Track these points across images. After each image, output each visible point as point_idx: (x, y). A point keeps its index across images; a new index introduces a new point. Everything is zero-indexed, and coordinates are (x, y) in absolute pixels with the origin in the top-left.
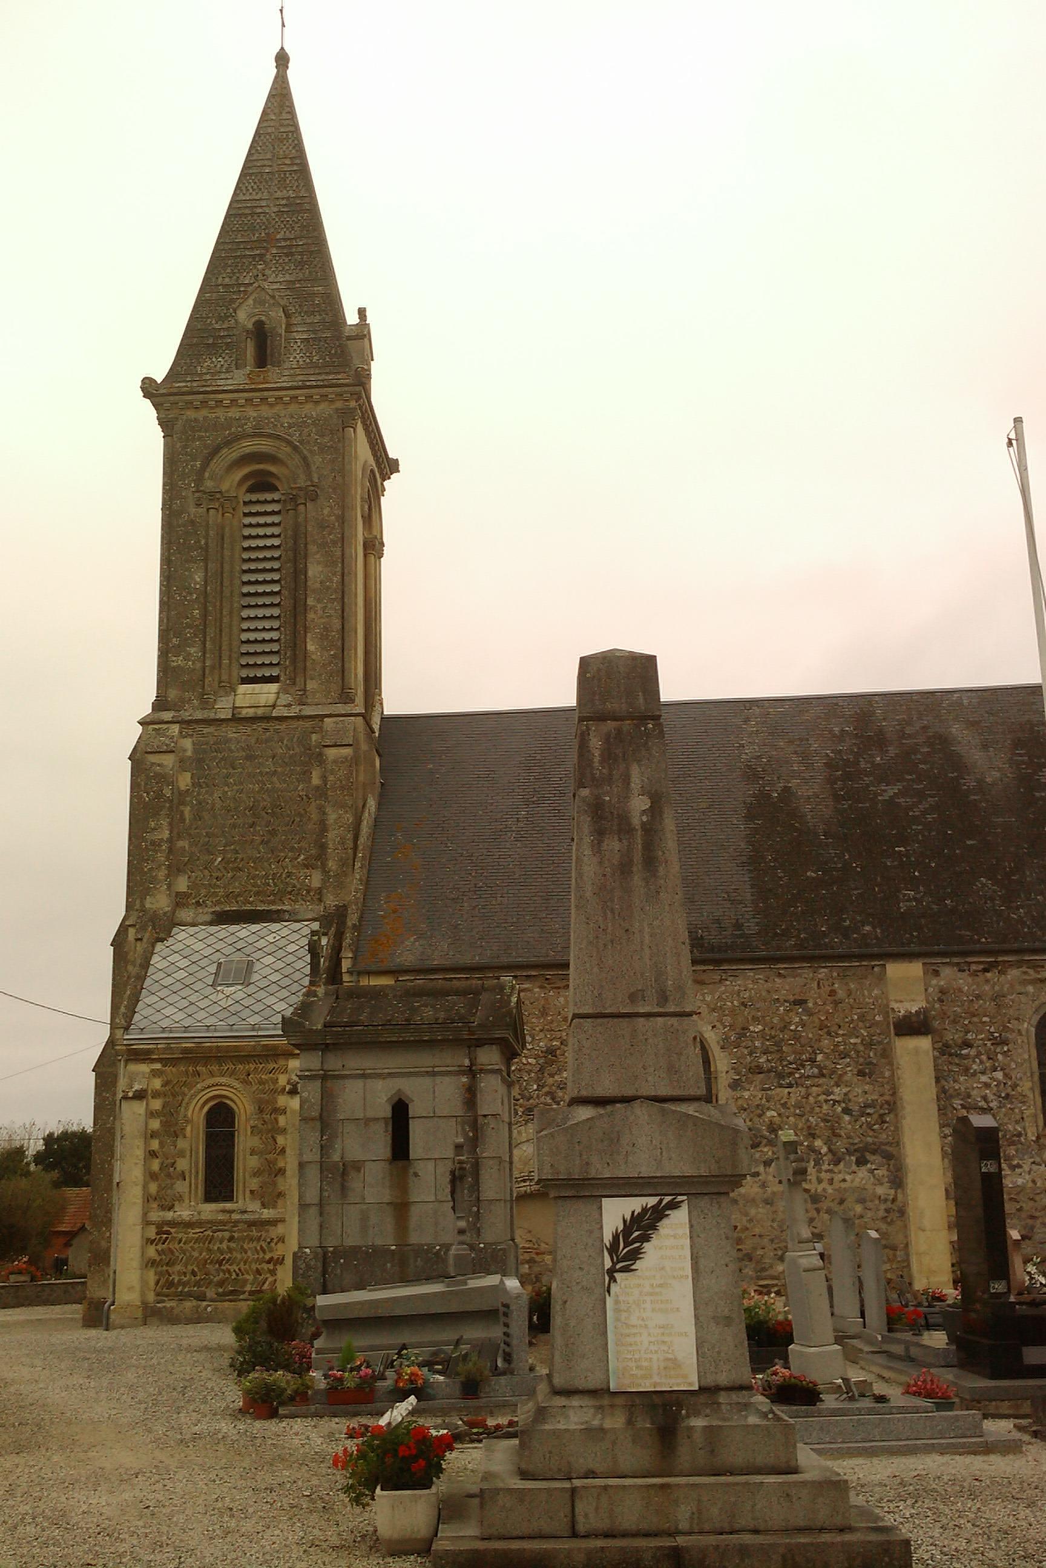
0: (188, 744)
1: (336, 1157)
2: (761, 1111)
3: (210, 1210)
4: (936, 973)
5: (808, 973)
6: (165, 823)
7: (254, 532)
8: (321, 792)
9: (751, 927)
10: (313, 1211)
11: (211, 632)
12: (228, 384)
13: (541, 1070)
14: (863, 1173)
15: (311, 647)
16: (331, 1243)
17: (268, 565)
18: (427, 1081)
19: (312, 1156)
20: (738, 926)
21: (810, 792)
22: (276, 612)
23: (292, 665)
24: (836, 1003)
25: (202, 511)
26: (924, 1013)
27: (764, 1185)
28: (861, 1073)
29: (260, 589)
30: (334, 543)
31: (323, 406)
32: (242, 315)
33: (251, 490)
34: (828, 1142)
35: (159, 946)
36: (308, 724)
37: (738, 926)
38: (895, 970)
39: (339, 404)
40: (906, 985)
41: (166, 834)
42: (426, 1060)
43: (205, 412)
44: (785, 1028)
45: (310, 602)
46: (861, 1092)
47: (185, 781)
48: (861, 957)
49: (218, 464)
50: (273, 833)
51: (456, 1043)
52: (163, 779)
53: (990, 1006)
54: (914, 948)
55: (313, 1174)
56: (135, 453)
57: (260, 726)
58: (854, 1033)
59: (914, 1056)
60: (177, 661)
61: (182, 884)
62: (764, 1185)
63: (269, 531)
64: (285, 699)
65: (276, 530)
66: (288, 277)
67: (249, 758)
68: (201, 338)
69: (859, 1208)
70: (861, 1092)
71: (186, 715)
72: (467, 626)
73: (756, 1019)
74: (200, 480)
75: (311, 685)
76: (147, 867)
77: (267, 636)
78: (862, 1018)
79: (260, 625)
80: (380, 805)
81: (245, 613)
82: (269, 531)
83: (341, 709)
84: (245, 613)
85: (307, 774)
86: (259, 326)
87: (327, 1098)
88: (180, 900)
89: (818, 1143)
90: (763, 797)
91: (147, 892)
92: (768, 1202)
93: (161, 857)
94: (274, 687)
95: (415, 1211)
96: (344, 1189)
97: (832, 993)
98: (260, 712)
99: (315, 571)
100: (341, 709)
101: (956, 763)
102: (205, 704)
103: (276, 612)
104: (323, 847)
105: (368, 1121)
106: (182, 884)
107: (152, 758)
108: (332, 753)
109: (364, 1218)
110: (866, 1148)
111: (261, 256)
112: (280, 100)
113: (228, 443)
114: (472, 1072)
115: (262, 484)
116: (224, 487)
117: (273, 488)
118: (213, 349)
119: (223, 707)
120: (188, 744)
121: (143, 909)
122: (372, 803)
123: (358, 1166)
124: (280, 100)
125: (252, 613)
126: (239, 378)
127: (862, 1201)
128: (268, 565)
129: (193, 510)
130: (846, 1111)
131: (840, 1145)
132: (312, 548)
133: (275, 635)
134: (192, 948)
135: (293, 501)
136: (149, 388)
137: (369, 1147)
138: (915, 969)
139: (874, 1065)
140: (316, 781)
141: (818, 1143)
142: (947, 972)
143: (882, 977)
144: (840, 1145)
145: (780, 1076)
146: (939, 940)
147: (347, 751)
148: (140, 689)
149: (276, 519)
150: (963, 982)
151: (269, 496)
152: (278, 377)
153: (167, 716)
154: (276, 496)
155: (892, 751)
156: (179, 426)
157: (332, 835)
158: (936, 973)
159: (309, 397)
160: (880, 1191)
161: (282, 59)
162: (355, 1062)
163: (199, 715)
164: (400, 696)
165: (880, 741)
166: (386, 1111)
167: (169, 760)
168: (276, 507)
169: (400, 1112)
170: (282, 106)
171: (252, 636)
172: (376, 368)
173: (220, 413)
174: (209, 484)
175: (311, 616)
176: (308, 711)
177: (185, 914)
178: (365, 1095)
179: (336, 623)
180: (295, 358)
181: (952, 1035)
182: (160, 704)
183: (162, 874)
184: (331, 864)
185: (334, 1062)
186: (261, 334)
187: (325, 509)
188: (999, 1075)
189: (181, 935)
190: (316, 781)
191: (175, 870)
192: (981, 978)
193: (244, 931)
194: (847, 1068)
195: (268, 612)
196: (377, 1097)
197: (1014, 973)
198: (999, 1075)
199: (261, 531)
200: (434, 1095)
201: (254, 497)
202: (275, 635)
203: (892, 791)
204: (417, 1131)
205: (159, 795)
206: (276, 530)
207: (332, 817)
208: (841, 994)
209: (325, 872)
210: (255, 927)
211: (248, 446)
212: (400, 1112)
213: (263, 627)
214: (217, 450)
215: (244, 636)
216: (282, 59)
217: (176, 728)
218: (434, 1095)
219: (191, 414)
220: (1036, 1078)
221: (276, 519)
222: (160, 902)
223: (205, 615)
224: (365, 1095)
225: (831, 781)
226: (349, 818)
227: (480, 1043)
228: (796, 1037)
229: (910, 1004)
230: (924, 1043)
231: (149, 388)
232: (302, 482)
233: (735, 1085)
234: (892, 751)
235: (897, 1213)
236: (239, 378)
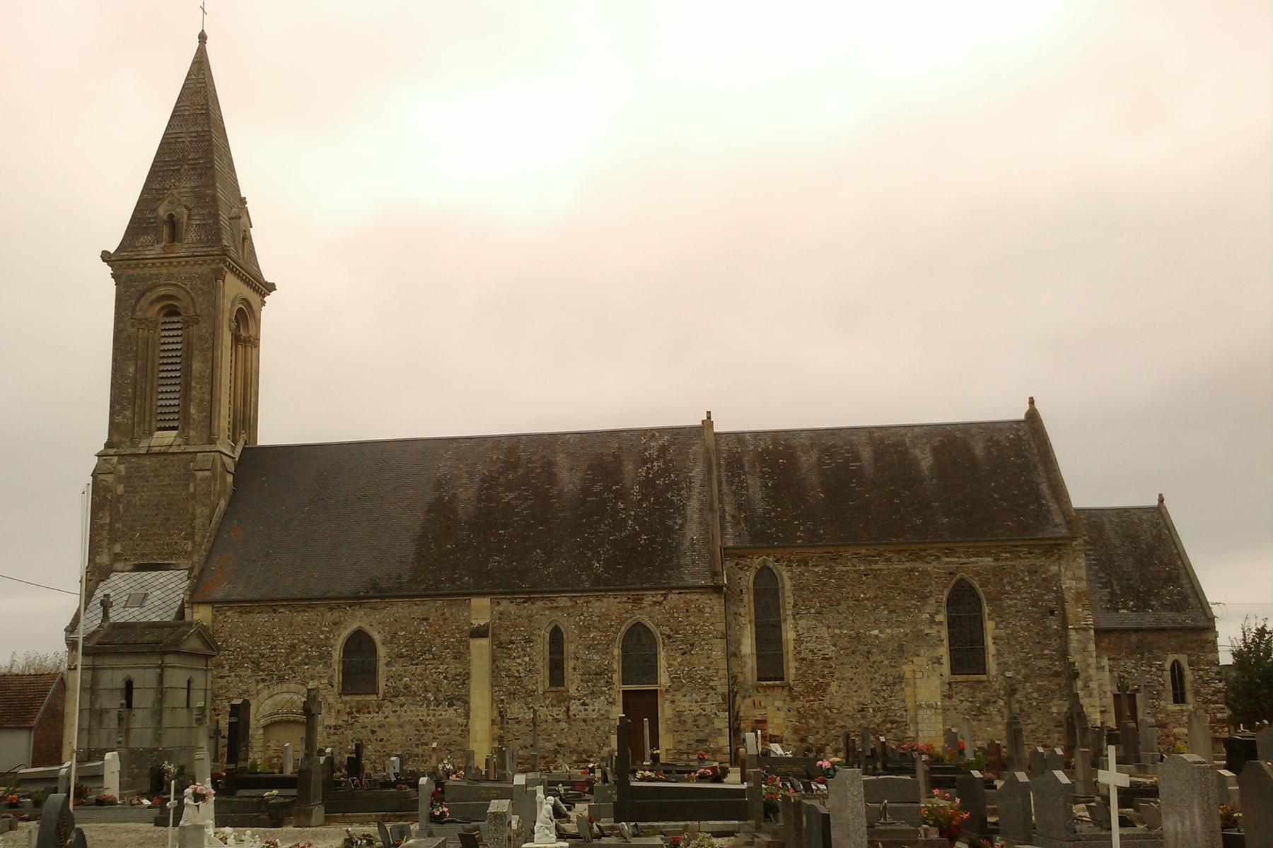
0: (122, 468)
1: (97, 707)
2: (401, 677)
3: (1178, 707)
4: (498, 603)
5: (431, 604)
6: (107, 514)
7: (166, 340)
8: (194, 496)
9: (406, 578)
10: (85, 733)
11: (138, 401)
12: (150, 253)
13: (287, 656)
14: (451, 711)
15: (193, 411)
16: (93, 747)
17: (174, 360)
18: (142, 671)
19: (87, 706)
20: (399, 577)
21: (467, 495)
22: (178, 388)
23: (182, 423)
24: (445, 620)
25: (135, 330)
26: (487, 625)
27: (399, 717)
28: (455, 658)
29: (169, 374)
30: (208, 349)
31: (205, 266)
32: (161, 211)
33: (166, 315)
34: (434, 694)
35: (101, 584)
36: (189, 456)
37: (399, 577)
38: (475, 602)
39: (213, 266)
40: (481, 610)
41: (108, 521)
42: (142, 661)
43: (137, 270)
44: (416, 633)
45: (193, 384)
46: (454, 668)
47: (120, 489)
48: (458, 595)
49: (144, 303)
50: (168, 520)
51: (153, 653)
52: (106, 488)
53: (525, 621)
54: (486, 590)
55: (86, 714)
56: (102, 290)
57: (162, 458)
58: (453, 636)
59: (480, 646)
60: (119, 419)
61: (118, 548)
62: (399, 717)
63: (175, 340)
64: (179, 441)
65: (179, 339)
66: (193, 184)
67: (156, 476)
68: (140, 224)
69: (448, 730)
70: (454, 668)
71: (122, 451)
72: (326, 375)
73: (402, 629)
74: (133, 312)
75: (192, 433)
76: (98, 538)
77: (172, 402)
78: (457, 627)
79: (168, 396)
80: (230, 504)
81: (160, 389)
82: (175, 340)
83: (207, 448)
84: (160, 389)
85: (187, 485)
86: (171, 216)
87: (95, 679)
88: (117, 557)
89: (429, 695)
90: (441, 498)
91: (97, 553)
92: (401, 726)
93: (105, 533)
94: (174, 433)
95: (132, 732)
96: (100, 722)
97: (443, 614)
98: (163, 449)
99: (197, 366)
100: (207, 448)
101: (552, 479)
102: (134, 445)
103: (178, 388)
104: (194, 528)
105: (112, 690)
106: (118, 548)
107: (102, 477)
108: (199, 474)
109: (109, 736)
110: (454, 698)
111: (178, 170)
112: (200, 66)
113: (150, 290)
114: (162, 667)
115: (173, 312)
116: (149, 315)
117: (178, 314)
118: (145, 231)
119: (143, 447)
120: (122, 468)
121: (95, 564)
122: (223, 503)
123: (107, 711)
124: (200, 66)
125: (164, 389)
126: (156, 250)
127: (450, 726)
128: (174, 360)
129: (129, 329)
130: (445, 678)
131: (441, 697)
132: (196, 352)
133: (176, 402)
134: (120, 584)
135: (187, 324)
136: (106, 256)
137: (111, 702)
138: (486, 601)
139: (461, 655)
140: (192, 490)
141: (429, 695)
142: (504, 603)
143: (469, 606)
144: (441, 697)
145: (413, 659)
146: (498, 587)
147: (207, 473)
148: (99, 434)
149: (179, 333)
150: (512, 609)
151: (176, 319)
152: (181, 250)
153: (111, 451)
154: (179, 319)
155: (520, 471)
156: (123, 278)
157: (199, 522)
158: (498, 603)
159: (196, 262)
160: (459, 720)
161: (203, 38)
162: (108, 661)
163: (129, 451)
164: (274, 429)
165: (514, 466)
166: (122, 685)
167: (110, 478)
168: (179, 326)
169: (129, 685)
170: (199, 70)
171: (163, 403)
172: (254, 232)
173: (146, 270)
174: (139, 314)
175: (194, 392)
176: (190, 449)
177: (118, 566)
178: (113, 678)
179: (207, 397)
180: (191, 236)
181: (504, 638)
182: (108, 445)
183: (105, 543)
184: (197, 538)
185: (98, 662)
186: (172, 222)
187: (204, 329)
188: (527, 659)
189: (115, 577)
190: (192, 490)
191: (113, 541)
192: (522, 606)
193: (148, 576)
194: (448, 654)
195: (173, 388)
196: (118, 679)
197: (539, 604)
198: (527, 659)
199: (171, 340)
200: (144, 678)
201: (167, 320)
202: (176, 402)
203: (512, 496)
204: (136, 694)
205: (105, 498)
206: (179, 339)
207: (198, 511)
208: (447, 614)
209: (194, 542)
210: (155, 573)
211: (161, 291)
212: (129, 685)
213: (168, 398)
214: (143, 294)
215: (160, 403)
216: (203, 38)
217: (115, 459)
218: (144, 678)
219: (130, 271)
220: (547, 660)
221: (179, 333)
222: (104, 559)
223: (134, 393)
224: (113, 678)
225: (480, 489)
226: (207, 512)
227: (165, 653)
228: (422, 637)
229: (480, 621)
230: (485, 642)
231: (106, 256)
232: (191, 313)
233: (388, 664)
234: (520, 471)
235: (465, 731)
236: (156, 250)
